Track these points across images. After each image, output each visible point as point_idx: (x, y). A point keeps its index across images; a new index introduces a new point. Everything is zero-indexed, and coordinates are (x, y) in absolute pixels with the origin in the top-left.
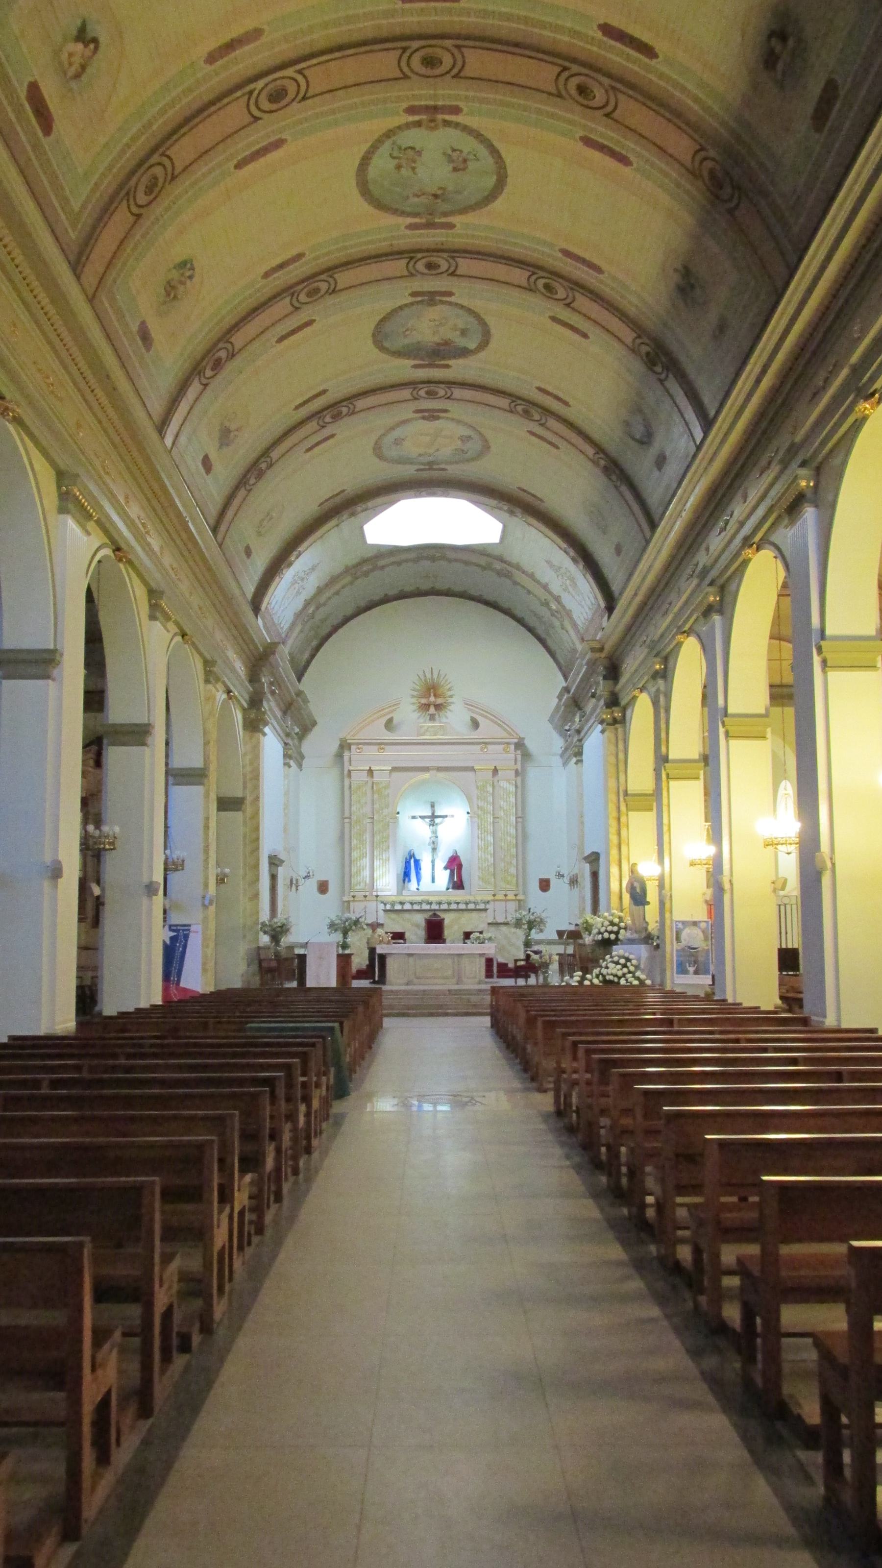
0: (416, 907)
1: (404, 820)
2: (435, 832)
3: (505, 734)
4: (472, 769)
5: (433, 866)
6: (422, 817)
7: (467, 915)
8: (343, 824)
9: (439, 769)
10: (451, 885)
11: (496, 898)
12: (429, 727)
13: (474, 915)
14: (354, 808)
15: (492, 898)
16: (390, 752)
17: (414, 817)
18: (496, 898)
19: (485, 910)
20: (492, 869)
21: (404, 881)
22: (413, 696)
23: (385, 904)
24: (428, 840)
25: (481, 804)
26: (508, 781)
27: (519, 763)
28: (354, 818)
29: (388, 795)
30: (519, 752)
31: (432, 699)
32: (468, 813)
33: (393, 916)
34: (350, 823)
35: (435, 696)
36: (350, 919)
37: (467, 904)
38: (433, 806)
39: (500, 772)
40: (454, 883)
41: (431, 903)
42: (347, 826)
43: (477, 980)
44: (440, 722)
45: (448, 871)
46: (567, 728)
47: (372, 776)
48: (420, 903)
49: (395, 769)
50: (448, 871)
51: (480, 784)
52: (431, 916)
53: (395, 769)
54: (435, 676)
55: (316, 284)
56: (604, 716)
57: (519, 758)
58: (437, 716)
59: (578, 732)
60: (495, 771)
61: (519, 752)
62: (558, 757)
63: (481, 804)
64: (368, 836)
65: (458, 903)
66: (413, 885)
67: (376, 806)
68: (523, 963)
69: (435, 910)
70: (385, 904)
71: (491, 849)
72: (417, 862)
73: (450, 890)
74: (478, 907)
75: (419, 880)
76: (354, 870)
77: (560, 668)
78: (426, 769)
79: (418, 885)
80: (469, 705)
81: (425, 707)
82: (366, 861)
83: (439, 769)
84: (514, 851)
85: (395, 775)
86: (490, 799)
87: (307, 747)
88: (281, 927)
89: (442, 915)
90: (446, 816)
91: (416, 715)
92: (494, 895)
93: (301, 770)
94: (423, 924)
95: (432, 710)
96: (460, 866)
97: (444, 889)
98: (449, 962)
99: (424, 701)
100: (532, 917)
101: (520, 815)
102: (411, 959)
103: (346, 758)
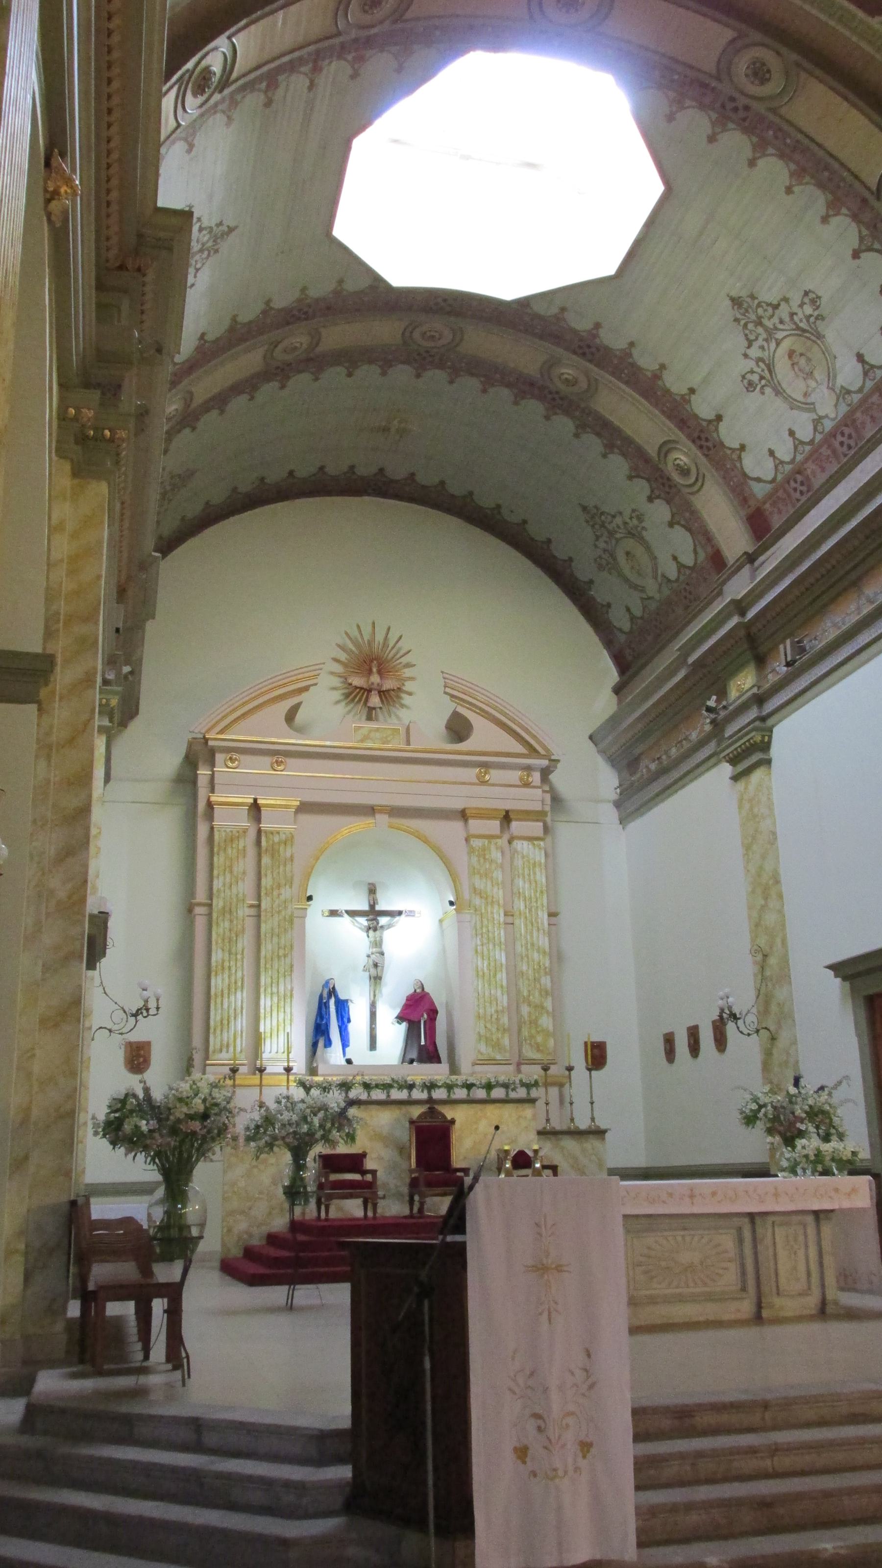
0: (378, 1095)
5: (373, 1015)
6: (352, 914)
10: (414, 1055)
14: (217, 884)
16: (294, 770)
17: (334, 913)
19: (532, 1101)
21: (315, 1045)
24: (362, 960)
28: (218, 903)
29: (292, 859)
31: (375, 679)
34: (210, 915)
35: (379, 672)
36: (324, 1108)
37: (489, 1087)
38: (372, 891)
40: (421, 1049)
42: (200, 923)
45: (404, 1026)
48: (387, 1087)
49: (305, 808)
53: (305, 808)
54: (380, 637)
63: (479, 883)
64: (245, 942)
66: (334, 1055)
67: (266, 882)
71: (502, 976)
72: (342, 1006)
74: (513, 1095)
75: (345, 1044)
76: (215, 1017)
78: (371, 810)
85: (304, 818)
89: (449, 1113)
90: (400, 913)
91: (341, 708)
95: (375, 700)
99: (357, 681)
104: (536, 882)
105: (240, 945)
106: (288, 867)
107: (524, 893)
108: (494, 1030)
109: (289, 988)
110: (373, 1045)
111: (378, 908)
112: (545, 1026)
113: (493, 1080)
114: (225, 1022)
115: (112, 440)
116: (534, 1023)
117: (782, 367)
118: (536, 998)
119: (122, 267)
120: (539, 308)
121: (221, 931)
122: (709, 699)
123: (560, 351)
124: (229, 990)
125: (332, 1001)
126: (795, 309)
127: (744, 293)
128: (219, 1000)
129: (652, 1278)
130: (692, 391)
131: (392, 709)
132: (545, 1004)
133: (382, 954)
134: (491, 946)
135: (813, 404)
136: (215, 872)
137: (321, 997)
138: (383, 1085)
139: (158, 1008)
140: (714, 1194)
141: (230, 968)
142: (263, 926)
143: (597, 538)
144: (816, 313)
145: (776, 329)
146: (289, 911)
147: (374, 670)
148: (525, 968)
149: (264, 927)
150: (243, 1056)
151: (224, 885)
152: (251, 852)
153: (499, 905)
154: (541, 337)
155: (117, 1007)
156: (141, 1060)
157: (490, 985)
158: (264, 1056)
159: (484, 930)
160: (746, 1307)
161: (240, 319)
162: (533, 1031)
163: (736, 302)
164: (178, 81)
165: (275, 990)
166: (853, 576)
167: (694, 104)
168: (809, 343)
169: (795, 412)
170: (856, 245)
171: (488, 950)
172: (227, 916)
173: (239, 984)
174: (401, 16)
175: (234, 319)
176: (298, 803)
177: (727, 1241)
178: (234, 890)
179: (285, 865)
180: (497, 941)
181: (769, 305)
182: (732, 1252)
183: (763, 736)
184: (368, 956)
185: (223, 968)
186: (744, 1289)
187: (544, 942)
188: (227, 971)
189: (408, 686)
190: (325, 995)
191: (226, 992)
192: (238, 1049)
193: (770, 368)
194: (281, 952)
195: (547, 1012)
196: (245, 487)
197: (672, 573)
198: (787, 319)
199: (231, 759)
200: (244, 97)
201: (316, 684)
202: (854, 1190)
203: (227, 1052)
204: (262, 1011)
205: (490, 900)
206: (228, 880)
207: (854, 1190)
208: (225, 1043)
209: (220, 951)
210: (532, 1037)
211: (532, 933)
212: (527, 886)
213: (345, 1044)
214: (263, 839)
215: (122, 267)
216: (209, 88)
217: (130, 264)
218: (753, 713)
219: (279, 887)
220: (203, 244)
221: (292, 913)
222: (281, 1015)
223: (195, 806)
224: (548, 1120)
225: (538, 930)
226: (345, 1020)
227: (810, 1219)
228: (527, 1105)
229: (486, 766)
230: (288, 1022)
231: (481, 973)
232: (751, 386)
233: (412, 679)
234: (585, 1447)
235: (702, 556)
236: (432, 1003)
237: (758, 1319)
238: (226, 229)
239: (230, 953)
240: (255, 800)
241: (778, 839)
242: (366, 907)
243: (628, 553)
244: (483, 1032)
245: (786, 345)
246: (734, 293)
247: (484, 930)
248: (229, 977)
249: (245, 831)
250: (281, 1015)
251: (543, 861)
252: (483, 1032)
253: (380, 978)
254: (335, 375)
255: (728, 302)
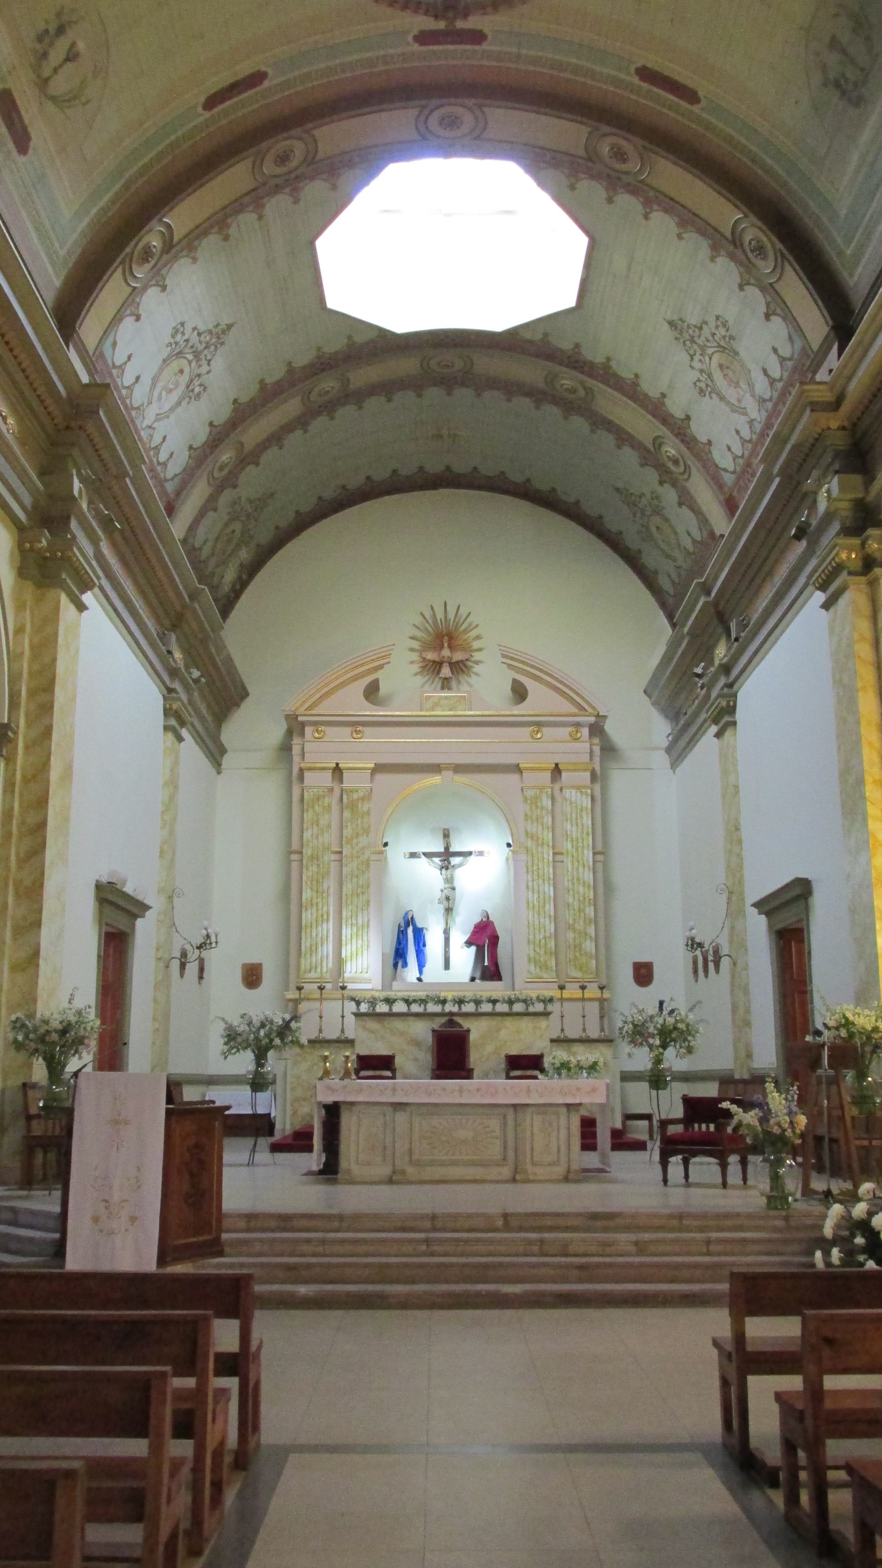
0: (415, 1008)
1: (396, 856)
2: (449, 880)
3: (574, 710)
4: (517, 769)
5: (447, 940)
6: (429, 855)
7: (510, 1024)
8: (289, 862)
9: (459, 769)
10: (478, 975)
11: (566, 994)
12: (441, 698)
13: (526, 1024)
14: (307, 835)
15: (557, 994)
16: (371, 737)
17: (413, 855)
18: (566, 994)
19: (546, 1014)
20: (552, 944)
21: (395, 965)
22: (412, 650)
23: (358, 1003)
24: (438, 894)
25: (532, 828)
26: (578, 788)
27: (597, 759)
28: (308, 852)
29: (368, 813)
30: (596, 741)
31: (446, 652)
32: (509, 845)
33: (372, 1024)
35: (450, 647)
38: (446, 835)
39: (564, 774)
41: (444, 1002)
42: (295, 866)
43: (560, 1170)
44: (459, 690)
45: (473, 949)
46: (699, 670)
47: (341, 781)
48: (423, 1001)
49: (379, 768)
50: (473, 949)
51: (529, 793)
52: (442, 1025)
53: (379, 768)
54: (451, 615)
55: (288, 142)
56: (844, 556)
57: (597, 750)
58: (454, 684)
59: (726, 669)
60: (557, 771)
61: (596, 741)
62: (663, 753)
63: (532, 828)
64: (331, 884)
65: (494, 1002)
66: (411, 972)
67: (347, 832)
68: (679, 1129)
69: (451, 1014)
70: (358, 1003)
71: (550, 908)
72: (419, 934)
73: (478, 981)
74: (531, 1009)
75: (421, 966)
76: (305, 944)
77: (663, 605)
78: (435, 768)
79: (421, 972)
80: (510, 659)
81: (434, 667)
82: (329, 928)
83: (459, 769)
84: (590, 911)
85: (382, 778)
86: (548, 820)
87: (230, 734)
88: (64, 1032)
89: (466, 1024)
90: (470, 853)
91: (420, 680)
92: (562, 988)
93: (219, 773)
94: (429, 1039)
95: (446, 671)
96: (494, 940)
97: (466, 979)
98: (494, 1124)
99: (431, 656)
100: (670, 1021)
101: (599, 848)
102: (401, 1118)
103: (296, 750)
104: (583, 825)
105: (325, 886)
106: (365, 820)
107: (572, 836)
108: (542, 953)
109: (366, 919)
110: (447, 966)
111: (452, 850)
112: (588, 949)
113: (513, 997)
114: (314, 948)
115: (62, 558)
116: (578, 947)
117: (718, 375)
118: (580, 925)
119: (68, 428)
120: (528, 336)
121: (310, 873)
122: (697, 667)
123: (558, 368)
124: (317, 921)
125: (410, 930)
126: (714, 330)
127: (675, 317)
128: (308, 930)
129: (434, 1148)
130: (664, 395)
131: (461, 678)
132: (588, 931)
133: (454, 889)
134: (541, 881)
135: (745, 408)
136: (305, 825)
137: (399, 926)
138: (420, 1000)
139: (217, 943)
140: (478, 1090)
141: (317, 904)
142: (344, 869)
143: (634, 515)
144: (728, 334)
145: (705, 346)
146: (366, 857)
147: (446, 645)
148: (571, 900)
149: (345, 870)
150: (328, 976)
151: (312, 835)
152: (335, 808)
153: (548, 845)
154: (537, 356)
155: (185, 942)
156: (254, 978)
157: (539, 915)
158: (346, 975)
159: (535, 868)
160: (506, 1172)
161: (268, 381)
162: (578, 954)
163: (672, 324)
164: (121, 263)
165: (354, 922)
166: (766, 569)
167: (586, 176)
168: (730, 358)
169: (736, 415)
170: (738, 280)
171: (538, 885)
172: (315, 861)
173: (325, 917)
174: (314, 158)
175: (262, 382)
176: (373, 765)
177: (494, 1124)
178: (321, 840)
179: (363, 818)
180: (546, 877)
181: (695, 326)
182: (498, 1133)
183: (728, 702)
184: (442, 891)
185: (312, 905)
186: (505, 1159)
187: (588, 877)
188: (315, 907)
189: (477, 656)
190: (403, 924)
191: (314, 923)
192: (325, 970)
193: (710, 376)
194: (359, 891)
195: (591, 937)
196: (329, 494)
197: (690, 547)
198: (710, 338)
199: (317, 731)
200: (200, 242)
201: (389, 663)
202: (594, 1090)
203: (316, 972)
204: (344, 938)
205: (540, 841)
206: (315, 832)
207: (594, 1090)
208: (314, 965)
209: (309, 891)
210: (576, 958)
211: (578, 869)
212: (574, 828)
213: (421, 966)
214: (345, 797)
215: (68, 428)
216: (152, 258)
217: (73, 424)
218: (722, 681)
219: (358, 835)
220: (207, 343)
221: (369, 857)
222: (360, 942)
223: (291, 772)
224: (562, 1030)
225: (584, 866)
226: (421, 945)
227: (564, 1110)
228: (541, 1018)
229: (539, 724)
230: (365, 947)
231: (531, 905)
232: (702, 392)
233: (480, 650)
234: (133, 1219)
235: (705, 534)
236: (494, 930)
237: (514, 1180)
238: (225, 327)
239: (317, 892)
240: (337, 764)
241: (741, 793)
242: (442, 850)
243: (658, 528)
244: (532, 954)
245: (716, 358)
246: (668, 317)
247: (535, 868)
248: (317, 910)
249: (331, 790)
250: (360, 942)
251: (589, 806)
252: (532, 954)
253: (451, 909)
254: (373, 403)
255: (666, 326)
